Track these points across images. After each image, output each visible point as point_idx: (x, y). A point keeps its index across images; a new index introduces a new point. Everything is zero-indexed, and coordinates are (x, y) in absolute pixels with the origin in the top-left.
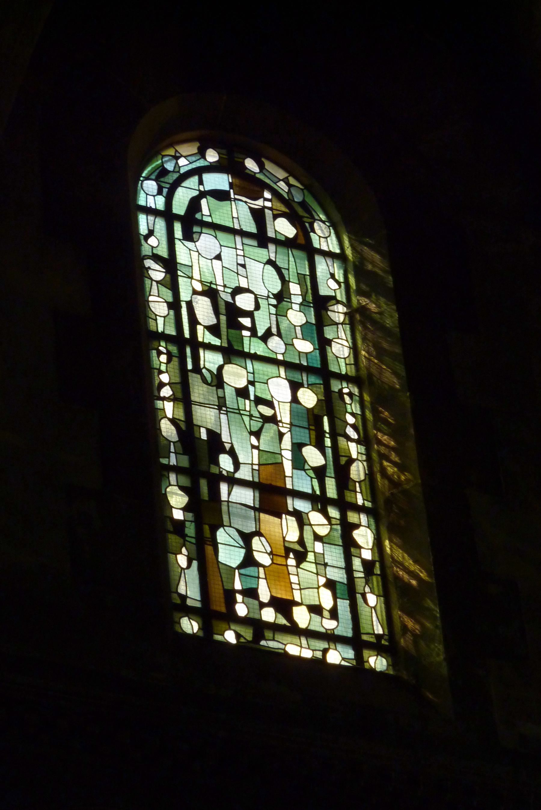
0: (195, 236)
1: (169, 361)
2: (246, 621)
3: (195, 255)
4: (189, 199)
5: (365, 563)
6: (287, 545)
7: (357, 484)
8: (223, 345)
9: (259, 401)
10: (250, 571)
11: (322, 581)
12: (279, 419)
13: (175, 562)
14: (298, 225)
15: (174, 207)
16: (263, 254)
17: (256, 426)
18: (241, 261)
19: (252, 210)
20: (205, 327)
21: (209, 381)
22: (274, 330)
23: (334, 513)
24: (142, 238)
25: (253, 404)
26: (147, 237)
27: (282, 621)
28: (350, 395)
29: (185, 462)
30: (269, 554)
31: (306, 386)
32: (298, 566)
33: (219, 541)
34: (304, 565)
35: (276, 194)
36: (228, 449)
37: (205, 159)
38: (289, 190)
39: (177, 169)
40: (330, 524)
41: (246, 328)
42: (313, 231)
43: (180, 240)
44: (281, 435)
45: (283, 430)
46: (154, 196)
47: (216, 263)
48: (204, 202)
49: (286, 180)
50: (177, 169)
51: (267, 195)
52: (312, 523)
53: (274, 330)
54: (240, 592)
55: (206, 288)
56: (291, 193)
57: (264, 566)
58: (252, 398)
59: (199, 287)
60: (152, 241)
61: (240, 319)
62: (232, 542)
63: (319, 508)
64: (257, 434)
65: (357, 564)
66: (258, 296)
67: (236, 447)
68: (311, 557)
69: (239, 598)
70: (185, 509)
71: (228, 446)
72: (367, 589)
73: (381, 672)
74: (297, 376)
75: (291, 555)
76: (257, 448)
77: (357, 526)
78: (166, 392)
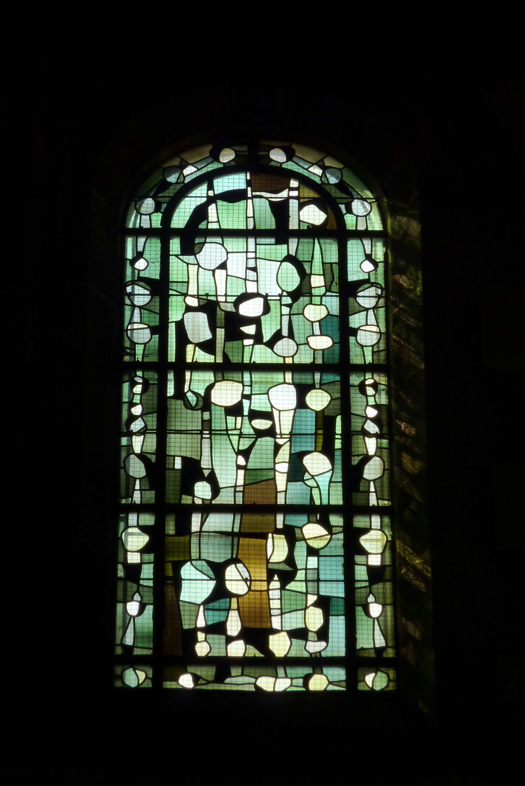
0: (196, 249)
1: (145, 390)
2: (207, 661)
3: (193, 269)
4: (194, 207)
5: (371, 570)
6: (270, 566)
7: (372, 484)
8: (217, 361)
9: (254, 415)
10: (223, 603)
11: (312, 599)
12: (278, 431)
13: (386, 464)
14: (329, 209)
15: (139, 523)
16: (282, 250)
17: (245, 444)
18: (251, 264)
19: (273, 205)
20: (196, 345)
21: (194, 403)
22: (285, 332)
23: (336, 520)
24: (128, 262)
25: (246, 420)
26: (133, 262)
27: (253, 652)
28: (375, 386)
29: (151, 496)
30: (246, 580)
31: (317, 386)
32: (283, 588)
33: (183, 577)
34: (292, 586)
35: (305, 181)
36: (206, 475)
37: (219, 161)
38: (324, 173)
39: (181, 180)
40: (331, 533)
41: (249, 337)
42: (349, 210)
43: (176, 256)
44: (277, 448)
45: (280, 441)
46: (150, 215)
47: (220, 274)
48: (212, 209)
49: (321, 163)
50: (181, 180)
51: (294, 183)
52: (306, 537)
53: (285, 332)
54: (202, 630)
55: (202, 302)
56: (326, 177)
57: (238, 596)
58: (246, 413)
59: (193, 302)
60: (141, 264)
61: (242, 328)
62: (200, 576)
63: (318, 518)
64: (246, 453)
65: (361, 573)
66: (269, 298)
67: (217, 472)
68: (300, 575)
69: (201, 636)
70: (143, 551)
71: (206, 473)
72: (371, 599)
73: (382, 691)
74: (305, 378)
75: (276, 578)
76: (244, 468)
77: (366, 531)
78: (137, 426)
